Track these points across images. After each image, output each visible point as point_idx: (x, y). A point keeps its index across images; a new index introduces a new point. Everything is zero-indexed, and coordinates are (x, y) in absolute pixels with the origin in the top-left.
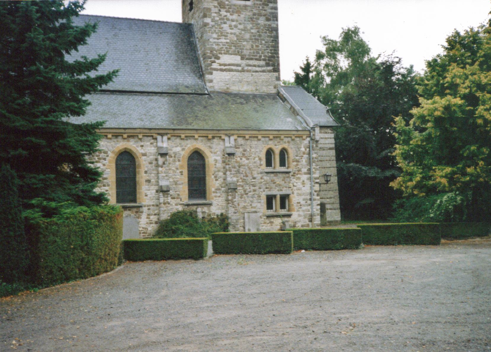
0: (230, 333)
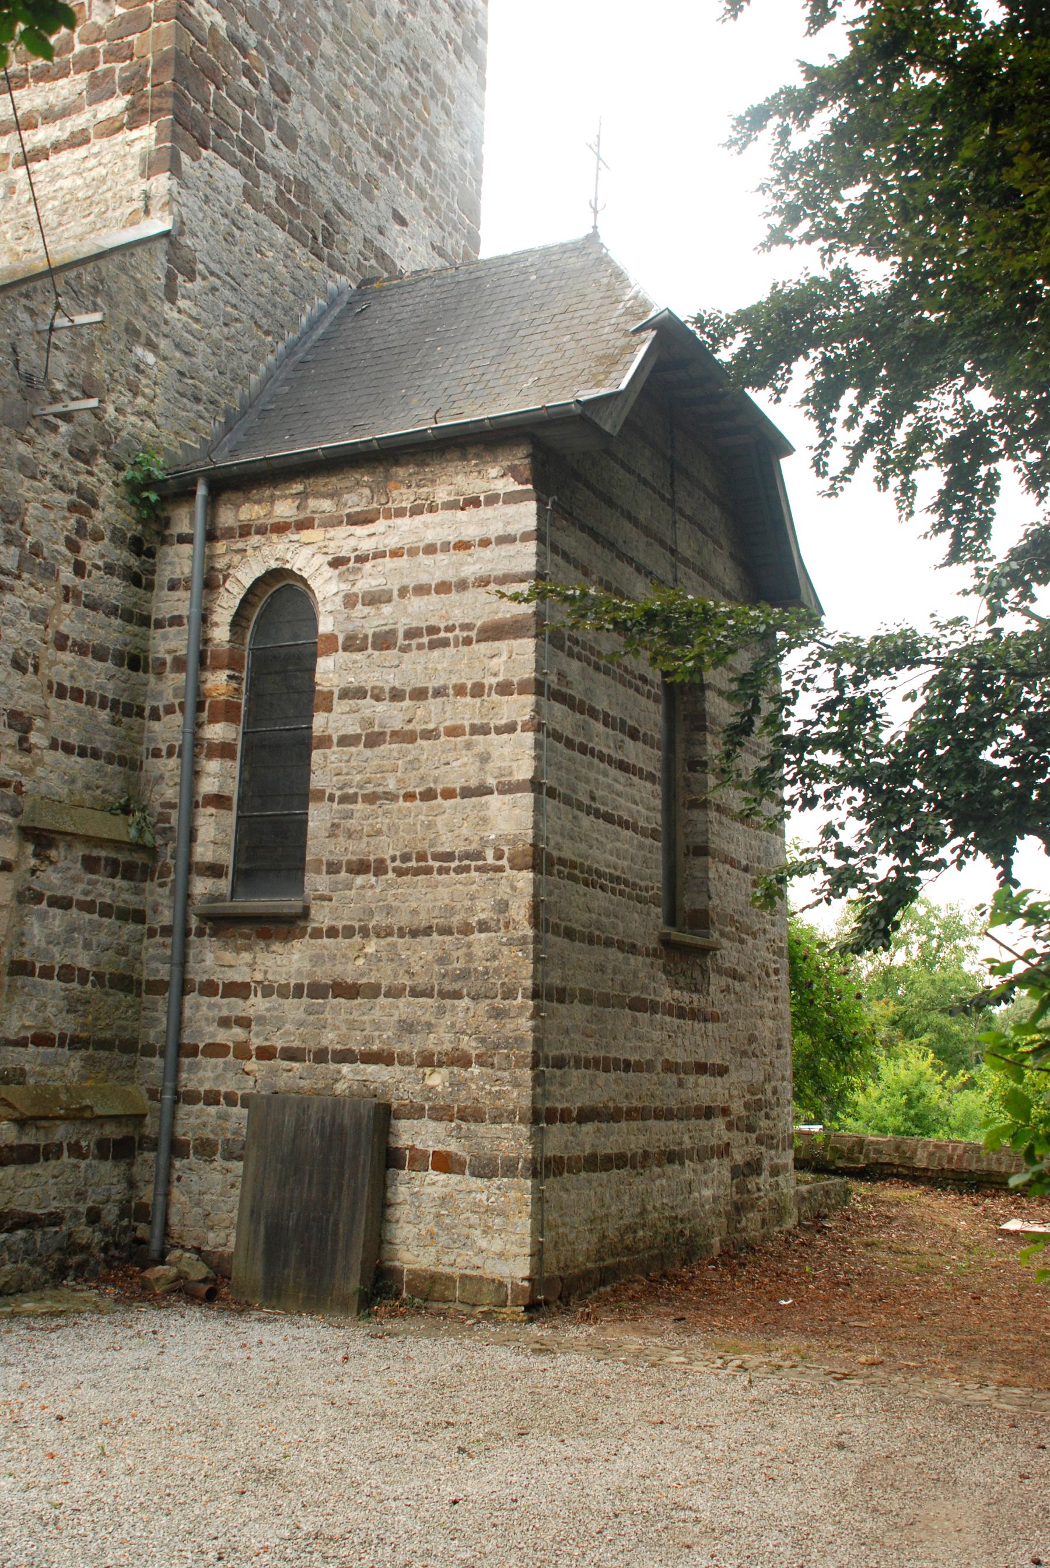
0: (764, 764)
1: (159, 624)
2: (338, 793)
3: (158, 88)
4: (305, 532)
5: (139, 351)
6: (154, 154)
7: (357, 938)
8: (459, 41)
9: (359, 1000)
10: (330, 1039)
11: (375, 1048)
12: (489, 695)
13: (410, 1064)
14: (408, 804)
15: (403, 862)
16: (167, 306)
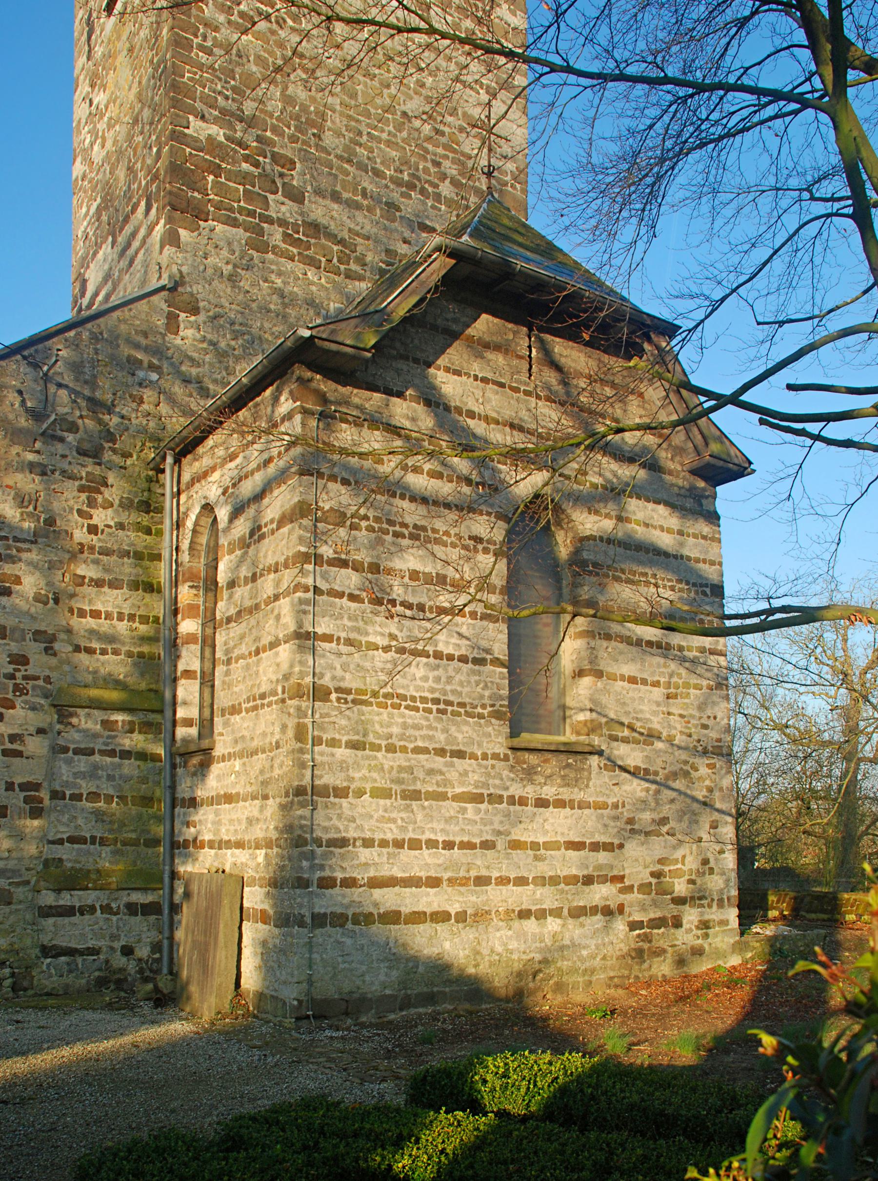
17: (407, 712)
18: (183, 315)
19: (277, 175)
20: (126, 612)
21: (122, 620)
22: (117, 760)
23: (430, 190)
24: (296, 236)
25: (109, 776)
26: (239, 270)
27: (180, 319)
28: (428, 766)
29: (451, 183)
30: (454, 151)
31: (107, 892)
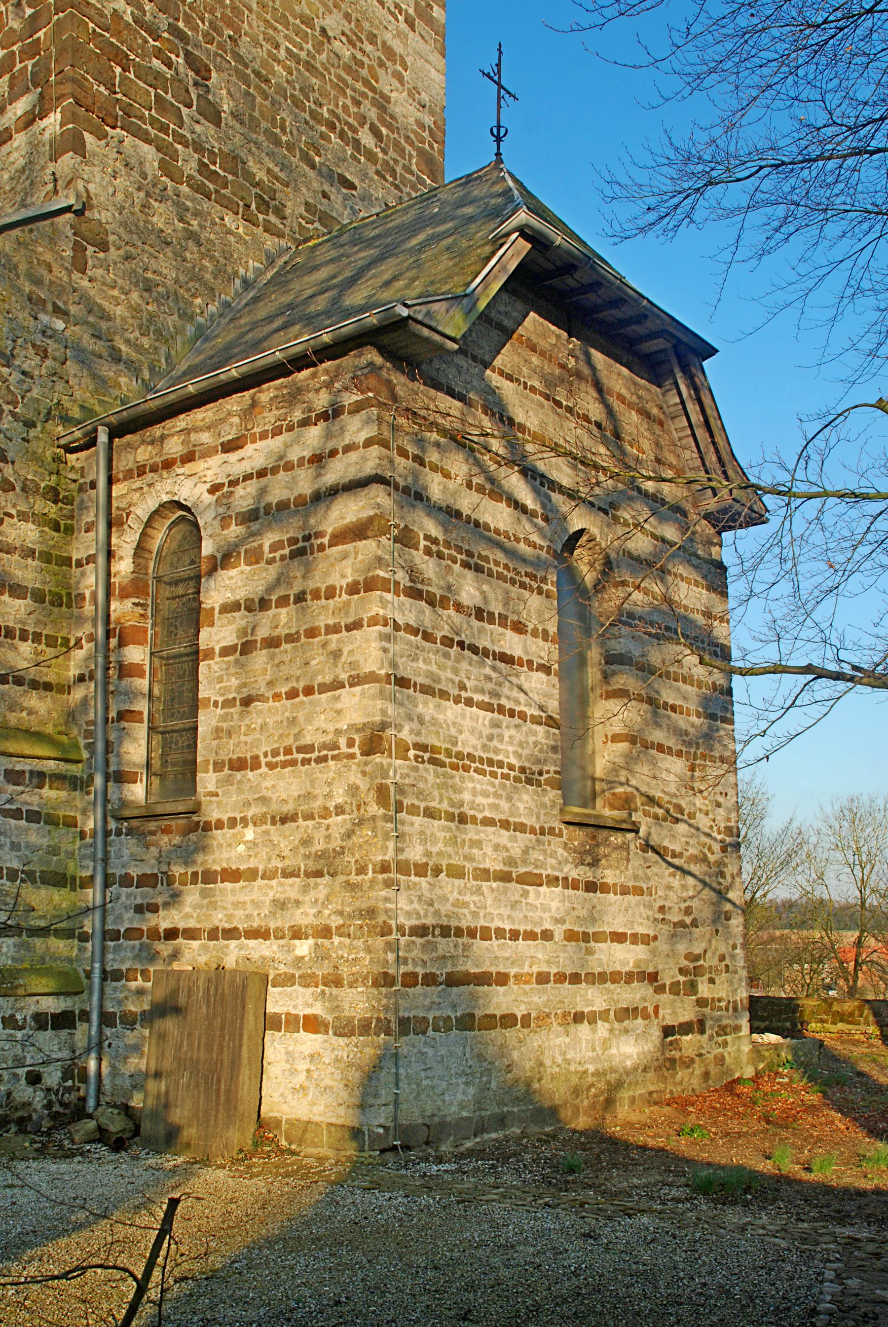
1: (79, 564)
2: (221, 699)
3: (60, 76)
4: (189, 465)
5: (44, 318)
6: (59, 138)
7: (239, 827)
8: (411, 11)
9: (242, 883)
10: (219, 919)
11: (255, 925)
12: (340, 596)
13: (282, 938)
14: (277, 704)
15: (273, 757)
16: (76, 276)
17: (475, 775)
18: (90, 249)
19: (191, 83)
20: (31, 629)
21: (26, 640)
22: (23, 823)
23: (350, 134)
24: (213, 168)
25: (13, 843)
26: (152, 201)
27: (87, 252)
28: (495, 840)
29: (370, 129)
30: (373, 89)
31: (12, 999)
